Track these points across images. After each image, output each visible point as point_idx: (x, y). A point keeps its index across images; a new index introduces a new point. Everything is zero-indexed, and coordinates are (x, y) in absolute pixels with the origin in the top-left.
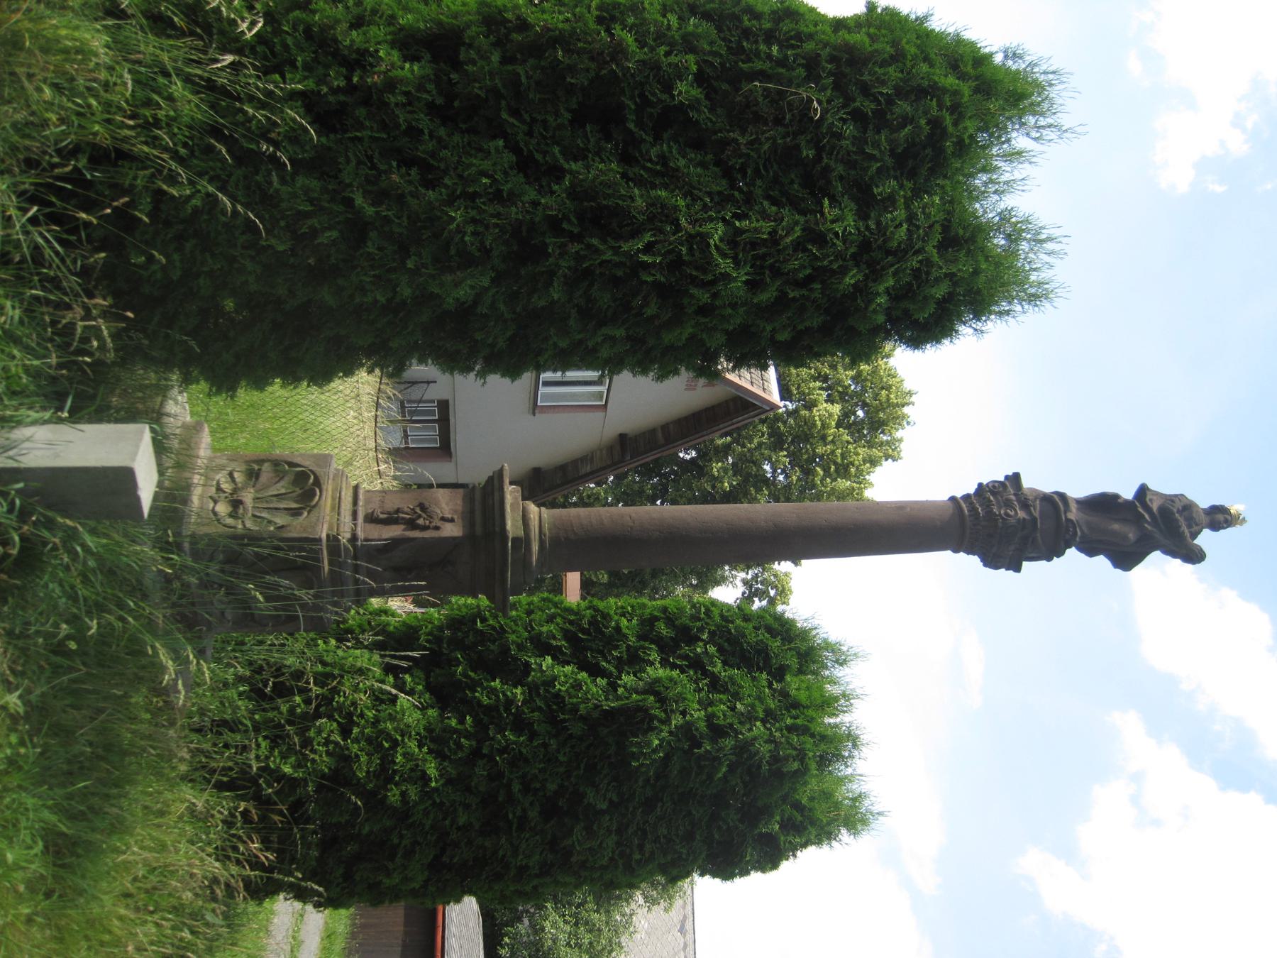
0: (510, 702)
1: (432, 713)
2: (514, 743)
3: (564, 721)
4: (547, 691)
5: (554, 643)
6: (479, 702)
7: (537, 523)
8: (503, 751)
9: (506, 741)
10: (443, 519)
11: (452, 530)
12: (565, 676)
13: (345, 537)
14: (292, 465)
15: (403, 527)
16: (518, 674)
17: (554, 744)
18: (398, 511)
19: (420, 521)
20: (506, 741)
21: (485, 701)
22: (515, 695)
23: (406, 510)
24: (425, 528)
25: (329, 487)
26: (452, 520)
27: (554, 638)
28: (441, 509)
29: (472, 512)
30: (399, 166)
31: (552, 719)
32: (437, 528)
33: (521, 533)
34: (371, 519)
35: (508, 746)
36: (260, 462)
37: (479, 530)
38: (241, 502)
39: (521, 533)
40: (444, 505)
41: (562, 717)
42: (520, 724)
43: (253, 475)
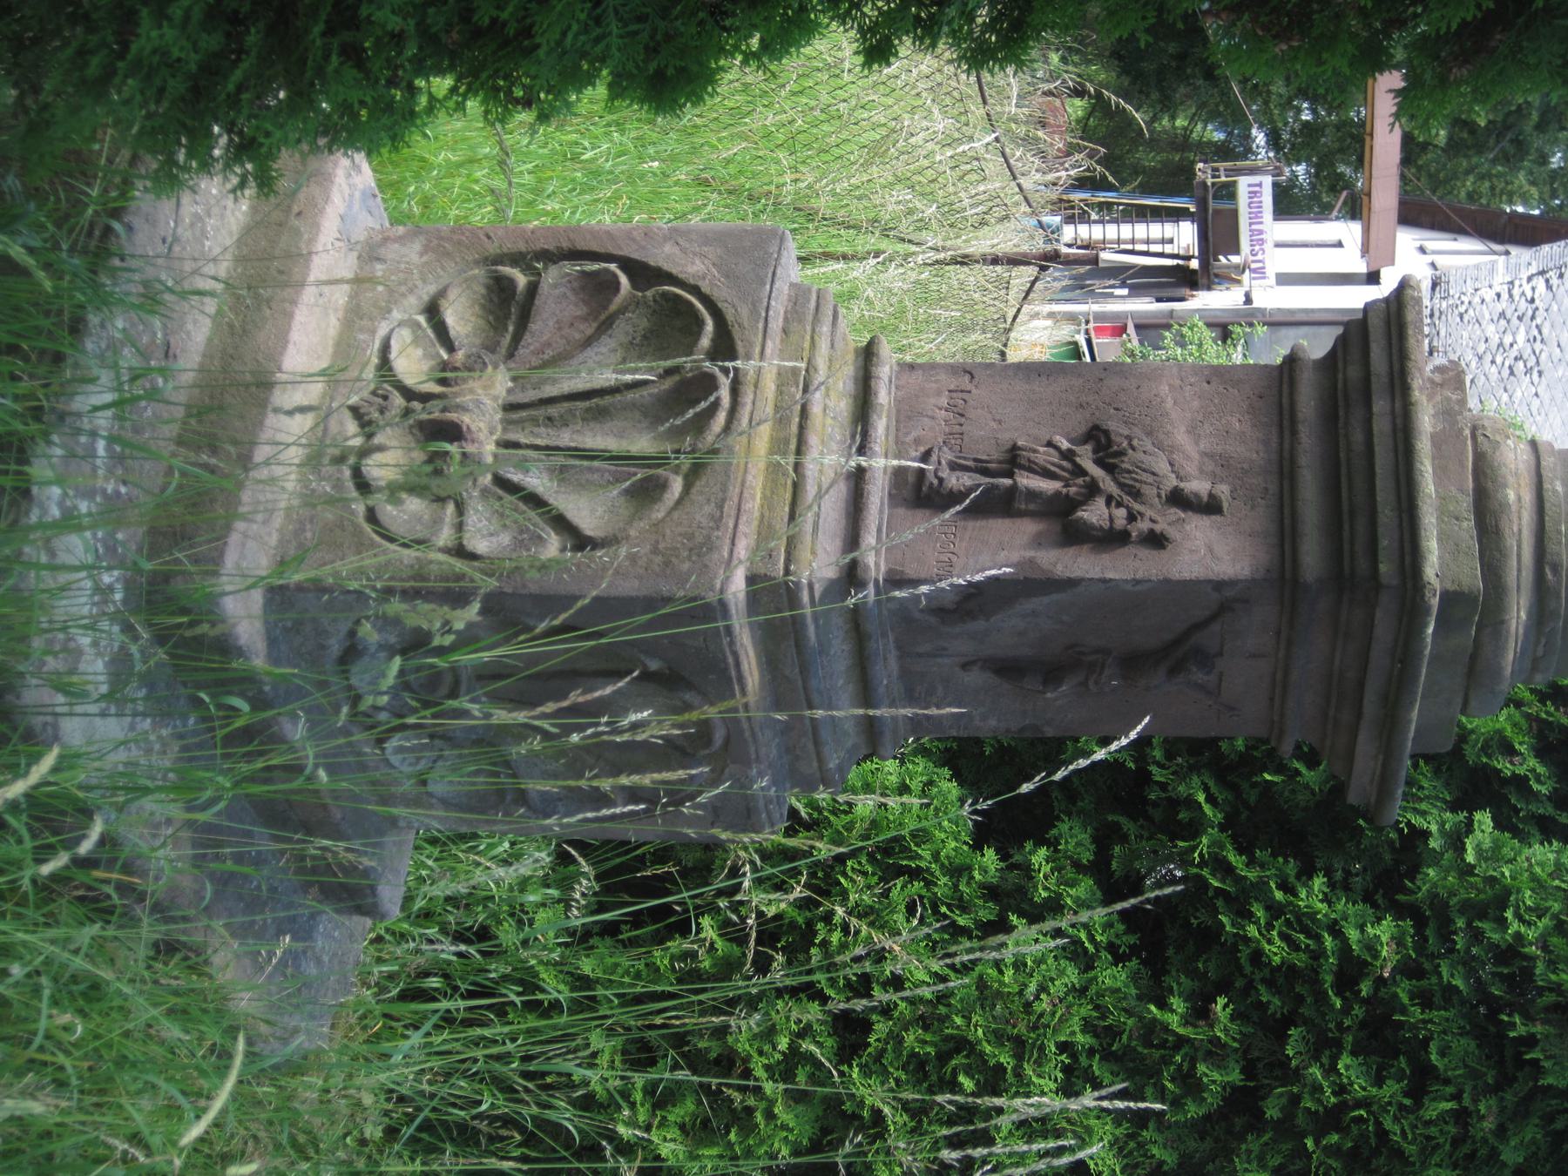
0: (1352, 969)
1: (1112, 976)
2: (1364, 1103)
3: (1530, 1041)
4: (1477, 936)
5: (1505, 766)
6: (1257, 956)
7: (1528, 497)
8: (1332, 1119)
9: (1341, 1090)
10: (1178, 499)
11: (1210, 552)
12: (1538, 884)
13: (819, 563)
14: (643, 274)
15: (1029, 527)
16: (1389, 877)
17: (1488, 1115)
18: (1014, 460)
19: (1095, 514)
20: (1341, 1090)
21: (1276, 951)
22: (1371, 947)
23: (1044, 456)
24: (1113, 539)
25: (764, 366)
26: (1211, 507)
27: (1509, 750)
28: (1170, 450)
29: (1285, 469)
30: (1174, 23)
31: (1485, 1027)
32: (1156, 541)
33: (1471, 576)
34: (919, 494)
35: (1342, 1107)
36: (539, 257)
37: (1312, 556)
38: (453, 432)
39: (1471, 576)
40: (1181, 437)
41: (1520, 1029)
42: (1382, 1038)
43: (508, 307)
